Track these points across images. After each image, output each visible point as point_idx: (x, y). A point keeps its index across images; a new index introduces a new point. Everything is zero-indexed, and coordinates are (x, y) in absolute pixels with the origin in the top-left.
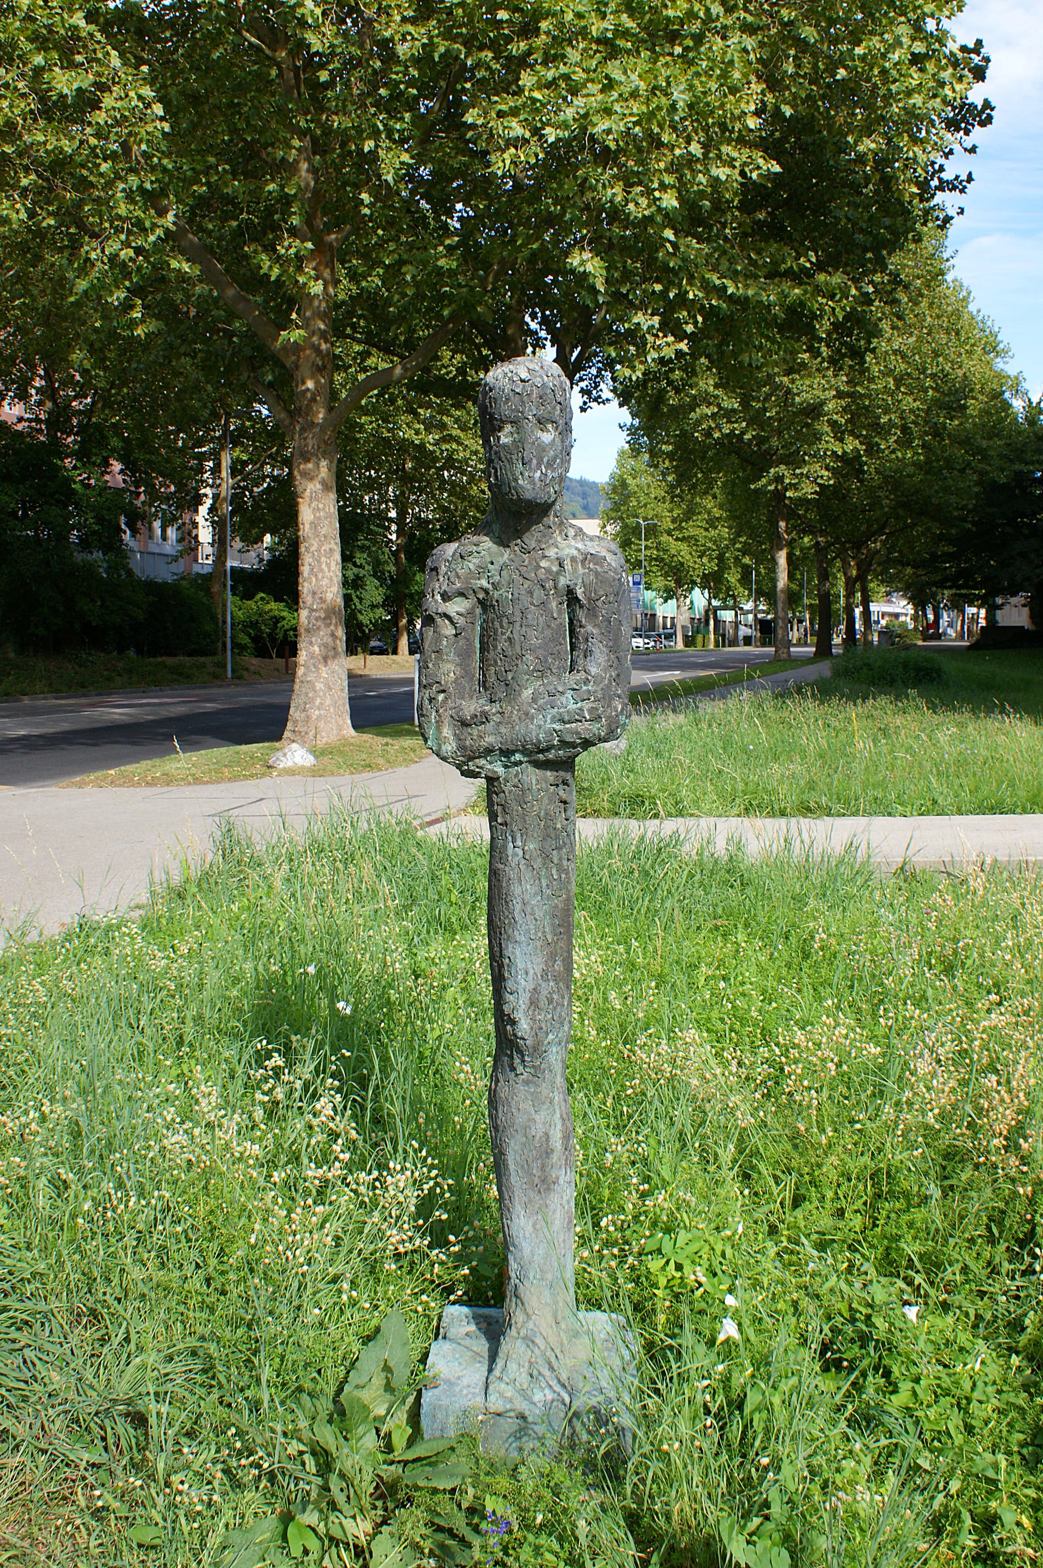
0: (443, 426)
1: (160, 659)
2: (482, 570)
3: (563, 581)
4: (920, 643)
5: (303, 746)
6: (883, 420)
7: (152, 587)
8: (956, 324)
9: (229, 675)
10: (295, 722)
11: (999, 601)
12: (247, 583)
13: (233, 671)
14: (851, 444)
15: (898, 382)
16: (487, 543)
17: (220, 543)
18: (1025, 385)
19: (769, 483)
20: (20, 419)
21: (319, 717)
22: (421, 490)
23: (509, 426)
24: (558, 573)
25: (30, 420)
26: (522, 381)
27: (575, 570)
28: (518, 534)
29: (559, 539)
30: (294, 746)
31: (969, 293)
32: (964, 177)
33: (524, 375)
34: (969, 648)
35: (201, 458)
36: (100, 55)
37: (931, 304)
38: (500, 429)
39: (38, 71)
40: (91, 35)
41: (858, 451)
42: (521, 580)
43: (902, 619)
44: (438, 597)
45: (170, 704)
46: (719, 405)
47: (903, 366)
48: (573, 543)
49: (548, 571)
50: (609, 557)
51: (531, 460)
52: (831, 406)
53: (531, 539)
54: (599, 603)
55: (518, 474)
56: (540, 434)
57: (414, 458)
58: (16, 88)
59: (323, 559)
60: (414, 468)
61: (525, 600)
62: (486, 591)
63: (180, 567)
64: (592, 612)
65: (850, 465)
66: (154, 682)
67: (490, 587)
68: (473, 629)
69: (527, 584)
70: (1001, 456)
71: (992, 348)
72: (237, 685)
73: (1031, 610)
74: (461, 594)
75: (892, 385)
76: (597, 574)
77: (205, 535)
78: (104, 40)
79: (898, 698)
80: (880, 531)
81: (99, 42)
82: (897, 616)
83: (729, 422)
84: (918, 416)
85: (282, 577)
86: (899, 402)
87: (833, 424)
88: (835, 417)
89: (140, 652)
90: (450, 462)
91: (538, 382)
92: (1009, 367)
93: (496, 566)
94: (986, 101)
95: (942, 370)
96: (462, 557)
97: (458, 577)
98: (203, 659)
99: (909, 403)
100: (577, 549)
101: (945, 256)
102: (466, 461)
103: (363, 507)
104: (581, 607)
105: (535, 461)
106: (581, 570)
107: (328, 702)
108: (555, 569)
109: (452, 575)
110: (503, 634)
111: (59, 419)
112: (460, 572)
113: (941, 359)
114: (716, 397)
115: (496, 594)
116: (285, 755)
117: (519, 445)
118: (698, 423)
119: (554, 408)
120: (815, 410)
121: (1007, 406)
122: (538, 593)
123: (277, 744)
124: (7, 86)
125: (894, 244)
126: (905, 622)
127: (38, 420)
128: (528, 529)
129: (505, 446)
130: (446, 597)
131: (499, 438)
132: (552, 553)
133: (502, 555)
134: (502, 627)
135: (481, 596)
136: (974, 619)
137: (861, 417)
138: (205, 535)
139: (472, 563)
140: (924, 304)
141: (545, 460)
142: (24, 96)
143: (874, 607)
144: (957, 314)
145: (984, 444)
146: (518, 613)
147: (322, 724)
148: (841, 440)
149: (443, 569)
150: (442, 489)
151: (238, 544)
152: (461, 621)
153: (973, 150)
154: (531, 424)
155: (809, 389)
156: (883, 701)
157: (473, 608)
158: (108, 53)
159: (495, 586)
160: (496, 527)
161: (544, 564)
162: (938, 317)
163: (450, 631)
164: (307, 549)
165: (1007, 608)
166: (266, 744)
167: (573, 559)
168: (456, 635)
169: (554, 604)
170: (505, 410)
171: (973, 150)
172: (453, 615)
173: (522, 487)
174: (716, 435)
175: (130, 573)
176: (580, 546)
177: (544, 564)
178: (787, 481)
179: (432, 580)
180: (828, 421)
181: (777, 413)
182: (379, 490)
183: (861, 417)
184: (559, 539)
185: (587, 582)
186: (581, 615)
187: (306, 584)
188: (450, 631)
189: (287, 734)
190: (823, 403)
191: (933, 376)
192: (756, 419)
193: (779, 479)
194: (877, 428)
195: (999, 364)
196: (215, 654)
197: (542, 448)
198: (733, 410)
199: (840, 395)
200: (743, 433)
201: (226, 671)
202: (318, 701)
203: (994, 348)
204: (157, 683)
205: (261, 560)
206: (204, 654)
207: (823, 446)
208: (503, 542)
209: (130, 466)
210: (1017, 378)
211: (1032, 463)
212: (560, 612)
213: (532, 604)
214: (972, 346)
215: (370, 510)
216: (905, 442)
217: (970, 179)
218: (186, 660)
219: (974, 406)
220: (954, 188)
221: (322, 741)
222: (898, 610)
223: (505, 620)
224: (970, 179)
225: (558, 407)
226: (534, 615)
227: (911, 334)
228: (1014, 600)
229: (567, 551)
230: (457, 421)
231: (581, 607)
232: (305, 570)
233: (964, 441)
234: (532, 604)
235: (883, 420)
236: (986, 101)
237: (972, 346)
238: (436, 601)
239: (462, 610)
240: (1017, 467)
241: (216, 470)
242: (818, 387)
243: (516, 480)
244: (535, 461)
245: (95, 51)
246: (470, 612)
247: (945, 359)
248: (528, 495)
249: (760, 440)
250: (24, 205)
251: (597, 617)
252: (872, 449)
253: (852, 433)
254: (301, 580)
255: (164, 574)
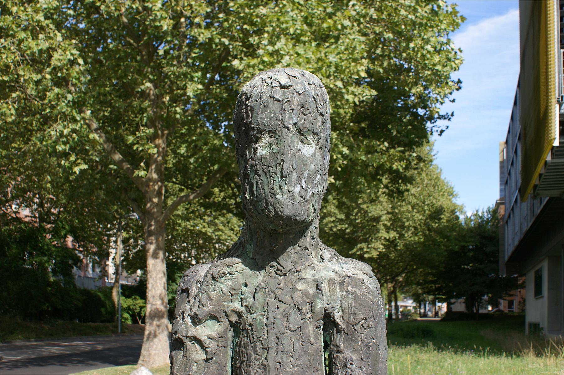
0: (216, 225)
1: (88, 324)
2: (234, 293)
3: (320, 305)
4: (419, 319)
5: (147, 368)
6: (407, 224)
7: (86, 293)
8: (436, 183)
9: (119, 331)
10: (144, 356)
11: (453, 300)
12: (127, 292)
13: (121, 329)
14: (393, 234)
15: (413, 208)
16: (238, 266)
17: (117, 273)
18: (465, 209)
19: (357, 251)
20: (26, 216)
21: (155, 354)
22: (206, 252)
23: (267, 136)
24: (315, 296)
25: (31, 217)
26: (282, 87)
27: (332, 293)
28: (274, 255)
29: (315, 261)
30: (143, 368)
31: (441, 170)
32: (450, 113)
33: (284, 81)
34: (440, 321)
35: (109, 236)
36: (52, 35)
37: (427, 174)
38: (257, 140)
39: (21, 41)
40: (48, 26)
41: (395, 237)
42: (277, 303)
43: (409, 308)
44: (188, 320)
45: (82, 345)
46: (336, 217)
47: (415, 200)
48: (330, 265)
49: (305, 293)
50: (366, 279)
51: (290, 174)
52: (384, 217)
53: (287, 260)
54: (358, 328)
55: (276, 188)
56: (300, 146)
57: (203, 239)
58: (10, 49)
59: (158, 281)
60: (203, 243)
61: (281, 324)
62: (239, 314)
63: (99, 284)
64: (351, 336)
65: (391, 244)
66: (81, 334)
67: (243, 310)
68: (225, 353)
69: (283, 307)
70: (456, 239)
71: (451, 194)
72: (123, 335)
73: (466, 304)
74: (213, 317)
75: (410, 209)
76: (356, 297)
77: (111, 270)
78: (54, 28)
79: (424, 346)
80: (402, 272)
81: (51, 29)
82: (406, 307)
83: (340, 224)
84: (421, 222)
85: (140, 290)
86: (414, 216)
87: (385, 225)
88: (386, 222)
89: (80, 321)
90: (219, 241)
91: (299, 88)
92: (458, 202)
93: (250, 289)
94: (459, 80)
95: (432, 203)
96: (214, 278)
97: (210, 299)
98: (108, 324)
99: (418, 217)
100: (334, 271)
101: (433, 154)
102: (226, 240)
103: (181, 259)
104: (339, 331)
105: (295, 175)
106: (339, 293)
107: (159, 347)
108: (312, 291)
109: (203, 297)
110: (256, 360)
111: (44, 217)
112: (212, 294)
113: (431, 198)
114: (335, 213)
115: (250, 318)
116: (138, 372)
117: (278, 158)
118: (327, 224)
119: (316, 119)
120: (377, 219)
121: (457, 218)
122: (295, 317)
123: (135, 366)
124: (5, 47)
125: (420, 144)
126: (410, 310)
127: (35, 217)
128: (284, 250)
129: (262, 158)
130: (196, 320)
131: (255, 150)
132: (308, 275)
133: (257, 277)
134: (256, 352)
135: (234, 318)
136: (440, 308)
137: (397, 223)
138: (111, 270)
139: (225, 285)
140: (424, 174)
141: (306, 173)
142: (13, 53)
143: (400, 303)
144: (438, 178)
145: (449, 234)
146: (273, 339)
147: (156, 357)
148: (388, 232)
149: (194, 291)
150: (215, 252)
151: (125, 274)
152: (212, 346)
153: (453, 101)
154: (291, 137)
155: (374, 210)
156: (414, 346)
157: (225, 332)
158: (56, 35)
159: (249, 310)
160: (250, 248)
161: (300, 286)
162: (430, 180)
163: (200, 355)
164: (151, 276)
165: (456, 304)
166: (130, 366)
167: (331, 282)
168: (207, 360)
169: (311, 328)
170: (263, 118)
171: (453, 101)
172: (203, 338)
173: (280, 203)
174: (335, 230)
175: (75, 285)
176: (337, 268)
177: (300, 286)
178: (365, 250)
179: (182, 300)
180: (383, 224)
181: (361, 221)
182: (188, 251)
183: (397, 223)
184: (315, 261)
185: (346, 305)
186: (339, 339)
187: (150, 293)
188: (199, 355)
189: (140, 362)
190: (380, 217)
191: (428, 205)
192: (352, 224)
193: (362, 249)
194: (403, 227)
195: (454, 200)
196: (114, 322)
197: (303, 162)
198: (342, 220)
199: (388, 213)
200: (346, 229)
201: (118, 330)
202: (155, 347)
203: (452, 194)
204: (86, 335)
205: (136, 281)
206: (109, 321)
207: (380, 235)
208: (257, 265)
209: (76, 239)
210: (462, 206)
211: (469, 242)
212: (316, 338)
213: (288, 328)
214: (444, 192)
215: (184, 261)
216: (415, 234)
217: (452, 115)
218: (101, 324)
219: (444, 217)
220: (445, 118)
221: (156, 365)
222: (407, 305)
223: (259, 345)
224: (452, 115)
225: (320, 118)
226: (289, 338)
227: (418, 187)
228: (460, 300)
229: (324, 273)
230: (222, 223)
231: (339, 331)
232: (149, 286)
233: (440, 232)
234: (288, 328)
235: (407, 224)
236: (459, 80)
237: (444, 192)
238: (186, 324)
239: (213, 334)
240: (463, 244)
241: (116, 242)
242: (381, 209)
243: (274, 195)
244: (295, 175)
245: (49, 33)
246: (222, 336)
247: (433, 197)
248: (287, 211)
249: (353, 232)
250: (13, 107)
251: (354, 341)
252: (401, 236)
253: (392, 229)
254: (147, 290)
255: (91, 286)
